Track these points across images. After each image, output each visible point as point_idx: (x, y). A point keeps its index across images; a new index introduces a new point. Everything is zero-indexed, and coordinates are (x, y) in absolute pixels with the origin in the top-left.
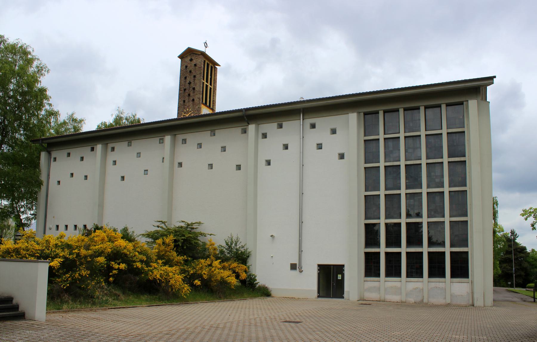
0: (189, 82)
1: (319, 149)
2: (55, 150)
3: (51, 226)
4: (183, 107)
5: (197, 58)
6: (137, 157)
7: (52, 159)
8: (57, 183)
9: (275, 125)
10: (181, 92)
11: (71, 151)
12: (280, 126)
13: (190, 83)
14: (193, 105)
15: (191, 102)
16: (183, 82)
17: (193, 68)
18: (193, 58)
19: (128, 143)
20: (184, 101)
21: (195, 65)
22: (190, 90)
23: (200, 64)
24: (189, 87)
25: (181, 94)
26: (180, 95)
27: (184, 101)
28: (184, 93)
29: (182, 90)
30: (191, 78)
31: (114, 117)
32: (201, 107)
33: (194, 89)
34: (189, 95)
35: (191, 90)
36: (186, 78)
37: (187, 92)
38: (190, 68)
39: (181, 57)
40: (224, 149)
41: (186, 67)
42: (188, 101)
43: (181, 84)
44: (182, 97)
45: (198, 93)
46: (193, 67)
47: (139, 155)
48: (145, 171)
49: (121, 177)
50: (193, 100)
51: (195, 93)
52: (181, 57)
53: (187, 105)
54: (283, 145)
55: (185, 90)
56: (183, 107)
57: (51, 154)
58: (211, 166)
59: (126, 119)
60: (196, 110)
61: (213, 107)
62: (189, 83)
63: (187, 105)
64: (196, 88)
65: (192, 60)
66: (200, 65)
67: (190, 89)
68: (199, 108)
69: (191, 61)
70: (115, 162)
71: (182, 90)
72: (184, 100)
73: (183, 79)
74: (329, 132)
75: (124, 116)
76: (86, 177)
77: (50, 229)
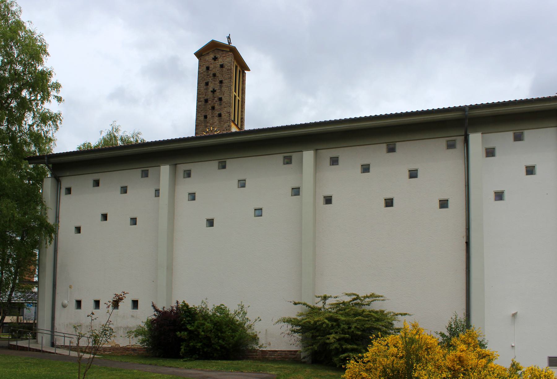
0: (212, 90)
1: (295, 195)
2: (68, 174)
3: (66, 302)
4: (203, 124)
5: (225, 57)
6: (238, 187)
7: (63, 191)
8: (75, 231)
9: (510, 135)
10: (200, 103)
11: (103, 177)
12: (391, 150)
13: (214, 91)
14: (220, 122)
15: (216, 119)
16: (202, 89)
17: (218, 70)
18: (218, 56)
19: (219, 164)
20: (206, 117)
21: (222, 66)
22: (215, 101)
23: (229, 64)
24: (213, 96)
25: (200, 106)
26: (199, 108)
27: (206, 117)
28: (205, 105)
29: (201, 101)
30: (215, 84)
31: (104, 134)
32: (231, 126)
33: (220, 99)
34: (213, 108)
35: (216, 101)
36: (207, 84)
37: (210, 104)
38: (214, 70)
39: (199, 54)
40: (413, 174)
41: (208, 68)
42: (212, 117)
43: (200, 92)
44: (201, 111)
45: (227, 105)
46: (218, 69)
47: (242, 184)
48: (255, 209)
49: (75, 227)
50: (220, 115)
51: (223, 106)
52: (199, 54)
53: (210, 122)
54: (526, 167)
55: (206, 101)
56: (203, 124)
57: (60, 182)
58: (389, 203)
59: (122, 139)
60: (225, 129)
61: (242, 127)
62: (212, 91)
63: (210, 122)
64: (223, 98)
65: (217, 58)
66: (229, 66)
67: (214, 100)
68: (229, 126)
69: (215, 60)
70: (192, 197)
71: (201, 101)
72: (206, 114)
73: (203, 84)
74: (359, 169)
75: (119, 135)
76: (134, 221)
77: (64, 306)
